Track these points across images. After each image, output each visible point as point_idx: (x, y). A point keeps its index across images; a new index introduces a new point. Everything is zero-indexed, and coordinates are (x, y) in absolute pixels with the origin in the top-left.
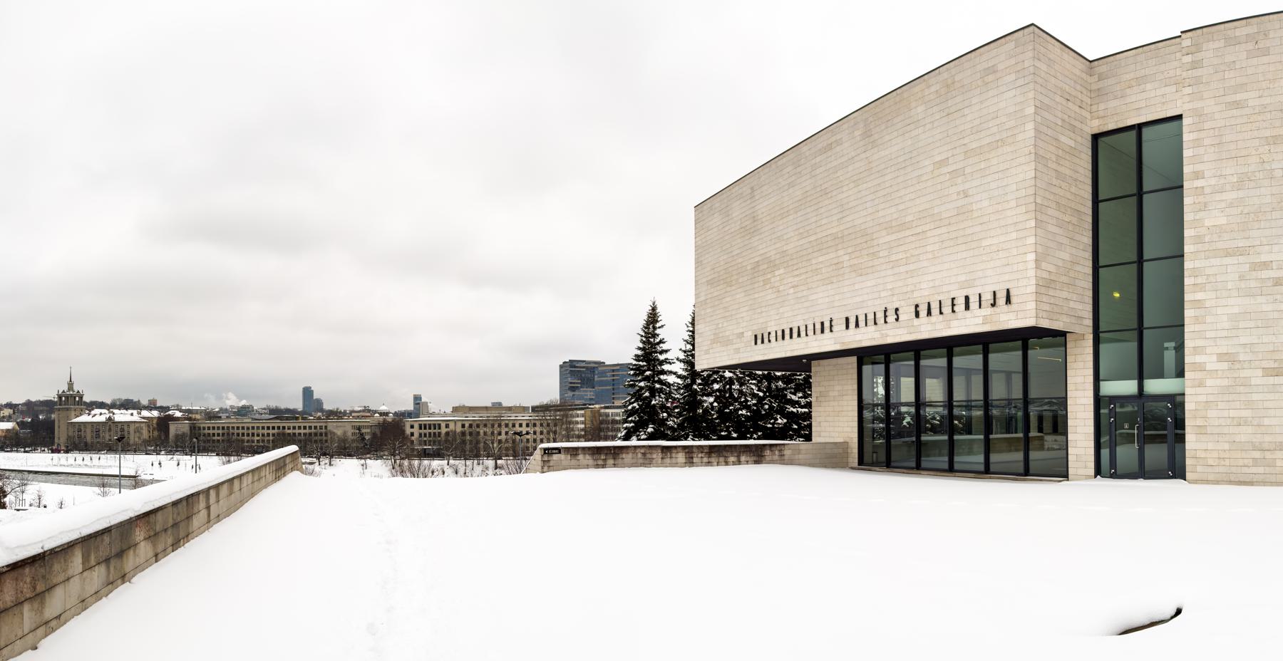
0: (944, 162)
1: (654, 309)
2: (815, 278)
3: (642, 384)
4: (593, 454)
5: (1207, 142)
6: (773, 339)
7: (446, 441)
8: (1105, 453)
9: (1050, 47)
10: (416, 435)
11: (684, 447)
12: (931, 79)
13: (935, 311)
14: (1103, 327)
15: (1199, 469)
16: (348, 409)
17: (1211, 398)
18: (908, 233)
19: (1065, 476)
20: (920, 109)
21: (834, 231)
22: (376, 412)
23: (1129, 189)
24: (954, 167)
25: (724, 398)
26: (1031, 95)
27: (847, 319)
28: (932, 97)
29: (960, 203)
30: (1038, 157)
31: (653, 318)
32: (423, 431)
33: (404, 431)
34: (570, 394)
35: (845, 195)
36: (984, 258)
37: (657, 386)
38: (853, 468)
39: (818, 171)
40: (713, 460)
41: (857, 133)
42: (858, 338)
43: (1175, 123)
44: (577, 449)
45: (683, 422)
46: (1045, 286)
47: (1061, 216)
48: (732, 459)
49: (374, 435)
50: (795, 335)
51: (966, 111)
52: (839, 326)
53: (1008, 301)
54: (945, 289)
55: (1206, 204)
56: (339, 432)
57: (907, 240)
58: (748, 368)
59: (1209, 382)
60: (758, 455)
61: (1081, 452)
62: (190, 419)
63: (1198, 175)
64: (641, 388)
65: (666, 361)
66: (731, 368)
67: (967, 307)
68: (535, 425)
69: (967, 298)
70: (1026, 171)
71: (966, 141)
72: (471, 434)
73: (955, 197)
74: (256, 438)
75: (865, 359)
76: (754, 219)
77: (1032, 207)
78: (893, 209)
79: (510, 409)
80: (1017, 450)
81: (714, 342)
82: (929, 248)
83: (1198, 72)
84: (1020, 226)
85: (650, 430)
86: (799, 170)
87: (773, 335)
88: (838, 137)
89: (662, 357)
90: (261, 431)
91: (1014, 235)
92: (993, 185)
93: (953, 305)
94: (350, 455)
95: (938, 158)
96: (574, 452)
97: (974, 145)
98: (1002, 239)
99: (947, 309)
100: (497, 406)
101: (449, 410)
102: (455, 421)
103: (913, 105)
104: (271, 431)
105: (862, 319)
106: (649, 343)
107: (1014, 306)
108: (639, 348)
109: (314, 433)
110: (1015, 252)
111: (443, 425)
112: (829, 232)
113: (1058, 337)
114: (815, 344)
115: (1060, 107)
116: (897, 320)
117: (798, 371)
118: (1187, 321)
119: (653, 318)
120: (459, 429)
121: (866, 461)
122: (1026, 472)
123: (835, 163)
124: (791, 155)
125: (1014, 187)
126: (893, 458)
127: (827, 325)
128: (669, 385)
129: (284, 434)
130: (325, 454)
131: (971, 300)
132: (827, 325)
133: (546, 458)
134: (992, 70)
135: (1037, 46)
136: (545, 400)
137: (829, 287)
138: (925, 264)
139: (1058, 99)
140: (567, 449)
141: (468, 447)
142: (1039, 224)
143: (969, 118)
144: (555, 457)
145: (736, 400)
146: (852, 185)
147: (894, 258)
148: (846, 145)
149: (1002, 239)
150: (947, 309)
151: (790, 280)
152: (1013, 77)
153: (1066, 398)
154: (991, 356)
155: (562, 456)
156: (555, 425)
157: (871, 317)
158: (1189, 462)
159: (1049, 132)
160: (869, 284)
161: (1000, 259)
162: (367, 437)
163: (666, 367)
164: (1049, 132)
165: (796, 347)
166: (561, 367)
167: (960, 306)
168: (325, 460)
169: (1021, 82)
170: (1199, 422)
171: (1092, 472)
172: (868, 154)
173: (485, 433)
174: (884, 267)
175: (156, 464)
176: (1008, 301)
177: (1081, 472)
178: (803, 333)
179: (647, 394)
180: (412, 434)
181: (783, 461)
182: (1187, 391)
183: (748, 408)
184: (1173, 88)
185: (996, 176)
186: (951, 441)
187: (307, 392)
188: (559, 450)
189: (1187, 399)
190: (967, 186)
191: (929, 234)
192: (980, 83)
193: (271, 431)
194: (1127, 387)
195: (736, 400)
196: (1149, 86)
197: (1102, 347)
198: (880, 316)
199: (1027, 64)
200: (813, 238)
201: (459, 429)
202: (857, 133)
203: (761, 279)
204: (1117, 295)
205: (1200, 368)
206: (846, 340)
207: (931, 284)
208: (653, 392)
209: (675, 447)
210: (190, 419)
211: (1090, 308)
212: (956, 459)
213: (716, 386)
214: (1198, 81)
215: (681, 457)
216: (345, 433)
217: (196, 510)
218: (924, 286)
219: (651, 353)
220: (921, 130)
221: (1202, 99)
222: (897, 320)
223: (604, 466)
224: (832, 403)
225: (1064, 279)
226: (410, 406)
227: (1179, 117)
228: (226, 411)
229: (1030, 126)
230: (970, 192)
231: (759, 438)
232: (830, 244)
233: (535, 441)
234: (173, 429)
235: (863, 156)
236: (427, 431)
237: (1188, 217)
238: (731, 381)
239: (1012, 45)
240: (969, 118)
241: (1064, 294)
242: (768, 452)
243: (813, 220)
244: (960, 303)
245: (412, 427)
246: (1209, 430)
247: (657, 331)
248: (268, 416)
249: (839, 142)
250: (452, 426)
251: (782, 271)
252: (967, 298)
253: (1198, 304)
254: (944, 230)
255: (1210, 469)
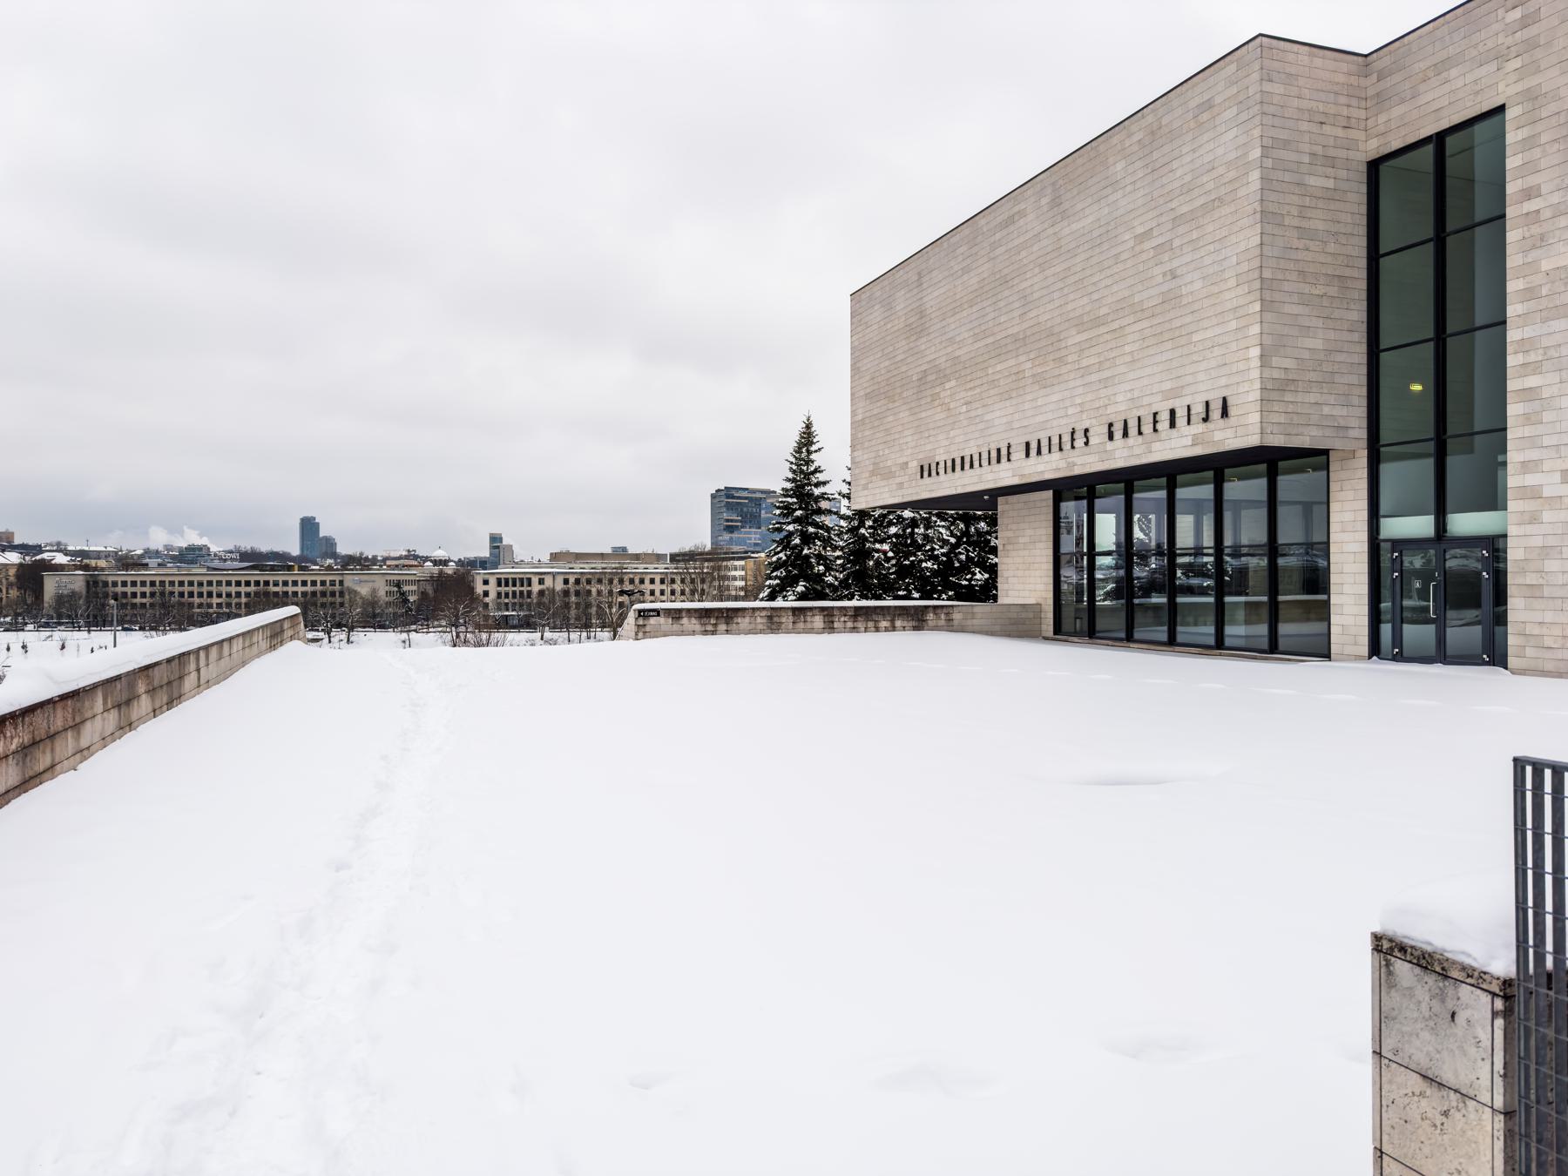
0: (1148, 234)
1: (808, 426)
2: (992, 392)
3: (791, 528)
4: (700, 617)
5: (1544, 138)
6: (941, 471)
7: (539, 604)
8: (1386, 630)
9: (1291, 57)
10: (493, 595)
11: (823, 609)
12: (1134, 126)
13: (1133, 431)
14: (1386, 435)
15: (1530, 652)
16: (380, 554)
17: (1551, 541)
18: (1103, 329)
19: (1326, 655)
20: (1119, 166)
21: (1015, 330)
22: (426, 559)
23: (1425, 218)
24: (1160, 240)
25: (905, 546)
26: (1257, 132)
27: (1028, 444)
28: (1135, 148)
29: (1165, 288)
30: (1268, 217)
31: (807, 439)
32: (503, 589)
33: (472, 590)
34: (727, 536)
35: (1029, 283)
36: (1195, 358)
37: (811, 530)
38: (1046, 638)
39: (998, 251)
40: (860, 625)
41: (1044, 201)
42: (1041, 468)
43: (1496, 119)
44: (680, 610)
45: (846, 579)
46: (1273, 391)
47: (1307, 289)
48: (884, 624)
49: (424, 594)
50: (967, 466)
51: (1175, 165)
52: (1019, 454)
53: (1225, 413)
54: (1146, 401)
55: (1542, 237)
56: (364, 590)
57: (1101, 340)
58: (938, 505)
59: (1547, 516)
60: (917, 619)
61: (1349, 621)
62: (86, 568)
63: (1529, 194)
64: (791, 534)
65: (823, 496)
66: (914, 505)
67: (1173, 424)
68: (673, 581)
69: (1173, 412)
70: (1251, 238)
71: (1173, 205)
72: (577, 593)
73: (1160, 279)
74: (215, 600)
75: (1065, 494)
76: (922, 314)
77: (1257, 284)
78: (1086, 300)
79: (637, 557)
80: (1259, 622)
81: (873, 473)
82: (1127, 349)
83: (1533, 30)
84: (1241, 312)
85: (800, 589)
86: (974, 250)
87: (942, 465)
88: (1022, 206)
89: (817, 492)
90: (224, 589)
91: (1233, 325)
92: (1208, 261)
93: (1155, 422)
94: (383, 627)
95: (1140, 230)
96: (676, 615)
97: (1185, 209)
98: (1218, 330)
99: (1147, 428)
100: (620, 553)
101: (546, 558)
102: (554, 575)
103: (1111, 160)
104: (243, 589)
105: (1045, 444)
106: (802, 472)
107: (1232, 420)
108: (788, 480)
109: (323, 592)
110: (1234, 347)
111: (535, 580)
112: (1010, 332)
113: (1317, 458)
114: (990, 477)
115: (1306, 138)
116: (1086, 443)
117: (976, 514)
118: (1510, 422)
119: (807, 439)
120: (559, 586)
121: (1060, 631)
122: (1273, 648)
123: (1016, 242)
124: (966, 231)
125: (1234, 259)
126: (1098, 627)
127: (1004, 452)
128: (828, 529)
129: (267, 594)
130: (339, 626)
131: (1167, 423)
132: (1004, 452)
133: (641, 622)
134: (1208, 105)
135: (1267, 63)
136: (687, 546)
137: (1008, 403)
138: (1122, 369)
139: (1304, 126)
140: (668, 612)
141: (573, 612)
142: (1266, 306)
143: (1179, 173)
144: (653, 621)
145: (919, 547)
146: (1037, 270)
147: (1085, 363)
148: (1031, 217)
149: (1218, 330)
150: (1147, 428)
151: (963, 394)
152: (1234, 110)
153: (1328, 543)
154: (1227, 486)
155: (661, 620)
156: (703, 581)
157: (1055, 441)
158: (1512, 640)
159: (1288, 177)
160: (1055, 398)
161: (1221, 352)
162: (412, 599)
163: (824, 505)
164: (1288, 177)
165: (966, 481)
166: (713, 497)
167: (1164, 424)
168: (339, 635)
169: (1244, 116)
170: (1531, 579)
171: (1365, 650)
172: (1057, 228)
173: (599, 593)
174: (1072, 376)
175: (16, 648)
176: (1225, 413)
177: (1349, 650)
178: (976, 464)
179: (797, 541)
180: (486, 594)
181: (950, 627)
182: (1512, 531)
183: (935, 558)
184: (1493, 66)
185: (1211, 248)
186: (1173, 606)
187: (309, 527)
188: (657, 612)
189: (1511, 543)
190: (1175, 263)
191: (1128, 330)
192: (1192, 125)
193: (243, 589)
194: (1420, 526)
195: (919, 547)
196: (1454, 72)
197: (1386, 469)
198: (1066, 439)
199: (1251, 91)
200: (990, 340)
201: (559, 586)
202: (1044, 201)
203: (929, 392)
204: (1417, 387)
205: (1533, 493)
206: (1026, 472)
207: (1129, 396)
208: (807, 539)
209: (811, 609)
210: (86, 568)
211: (1362, 412)
212: (1179, 629)
213: (893, 530)
214: (1532, 45)
215: (818, 621)
216: (374, 591)
217: (88, 714)
218: (1120, 398)
219: (803, 486)
220: (1119, 194)
221: (1538, 71)
222: (1086, 443)
223: (714, 633)
224: (1021, 553)
225: (1313, 376)
226: (485, 552)
227: (1501, 109)
228: (157, 553)
229: (1255, 175)
230: (1179, 272)
231: (949, 599)
232: (1010, 347)
233: (611, 593)
234: (51, 585)
235: (1051, 231)
236: (510, 589)
237: (1513, 260)
238: (914, 523)
239: (1233, 67)
240: (1179, 173)
241: (1312, 398)
242: (931, 616)
243: (992, 315)
244: (1164, 417)
245: (486, 582)
246: (1547, 592)
247: (813, 457)
248: (237, 564)
249: (1022, 214)
250: (548, 582)
251: (953, 383)
252: (1173, 412)
253: (1529, 394)
254: (1145, 324)
255: (1548, 654)
